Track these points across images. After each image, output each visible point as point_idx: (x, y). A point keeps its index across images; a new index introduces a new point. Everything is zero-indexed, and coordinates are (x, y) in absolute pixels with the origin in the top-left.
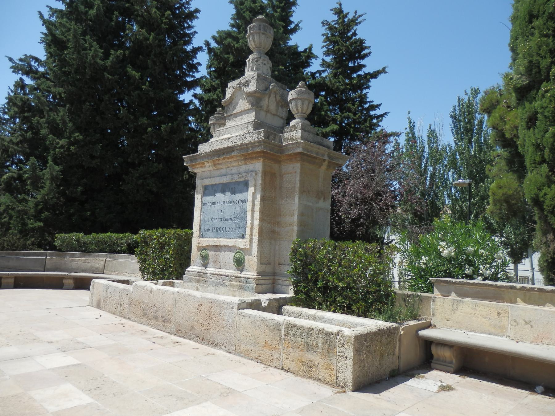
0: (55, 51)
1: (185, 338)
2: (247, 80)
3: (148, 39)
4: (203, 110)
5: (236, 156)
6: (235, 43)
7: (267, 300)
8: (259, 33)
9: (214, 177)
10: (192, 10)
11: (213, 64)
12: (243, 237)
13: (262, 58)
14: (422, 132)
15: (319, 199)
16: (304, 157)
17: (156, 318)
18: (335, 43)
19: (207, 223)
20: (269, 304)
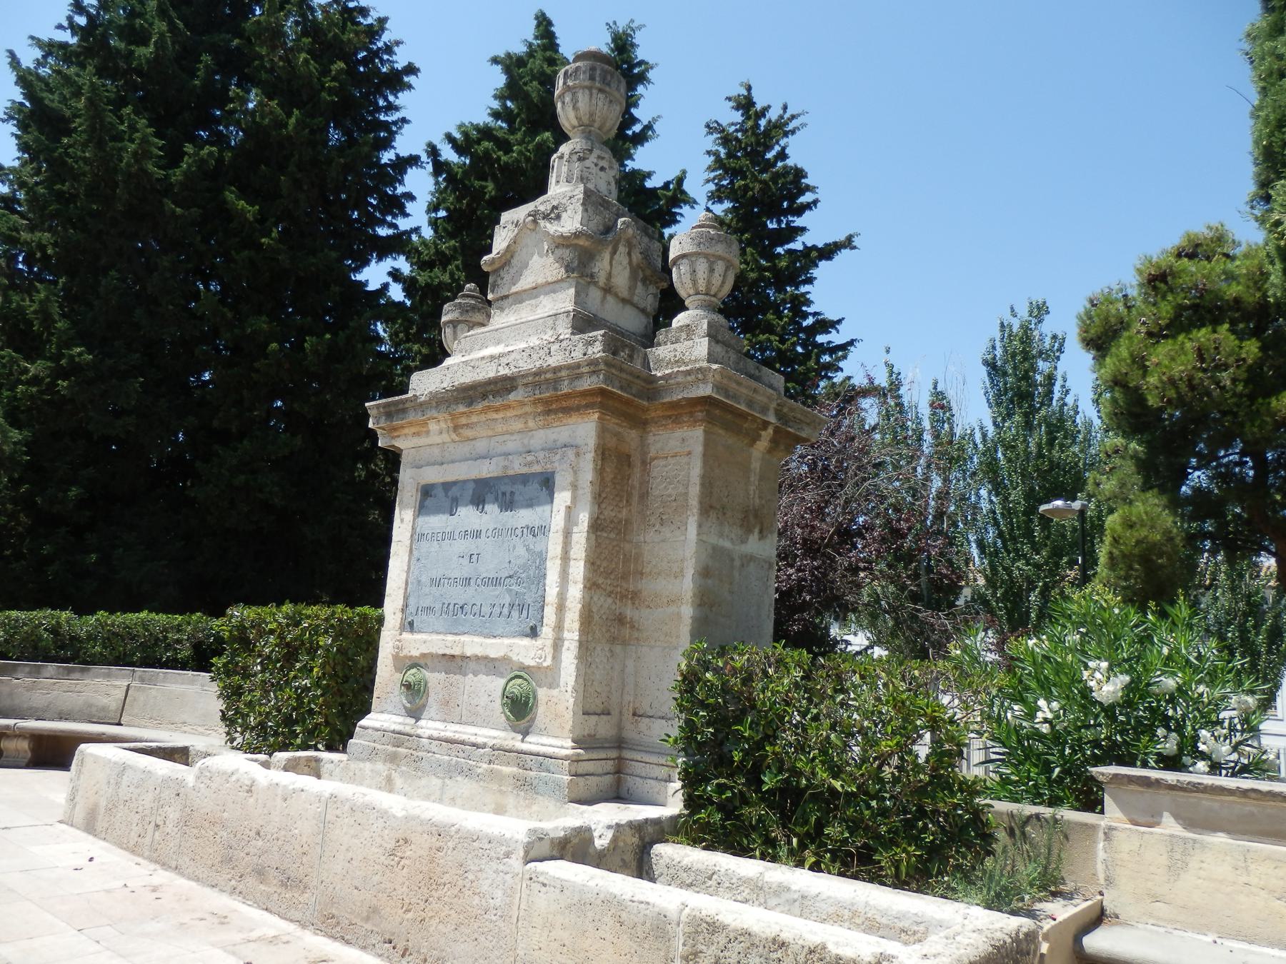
0: (36, 140)
1: (348, 943)
2: (555, 203)
3: (285, 126)
4: (413, 308)
5: (522, 404)
6: (501, 153)
7: (609, 827)
8: (590, 88)
9: (453, 462)
10: (399, 66)
11: (444, 200)
12: (533, 633)
13: (596, 152)
14: (917, 397)
15: (749, 531)
16: (715, 412)
17: (260, 873)
18: (735, 173)
19: (427, 590)
20: (615, 840)
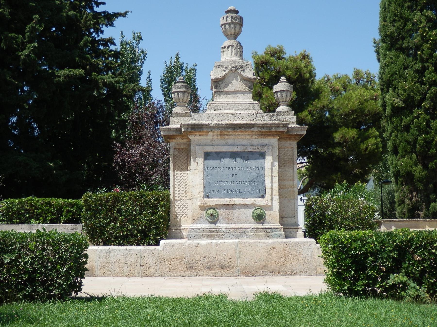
12: (263, 197)
